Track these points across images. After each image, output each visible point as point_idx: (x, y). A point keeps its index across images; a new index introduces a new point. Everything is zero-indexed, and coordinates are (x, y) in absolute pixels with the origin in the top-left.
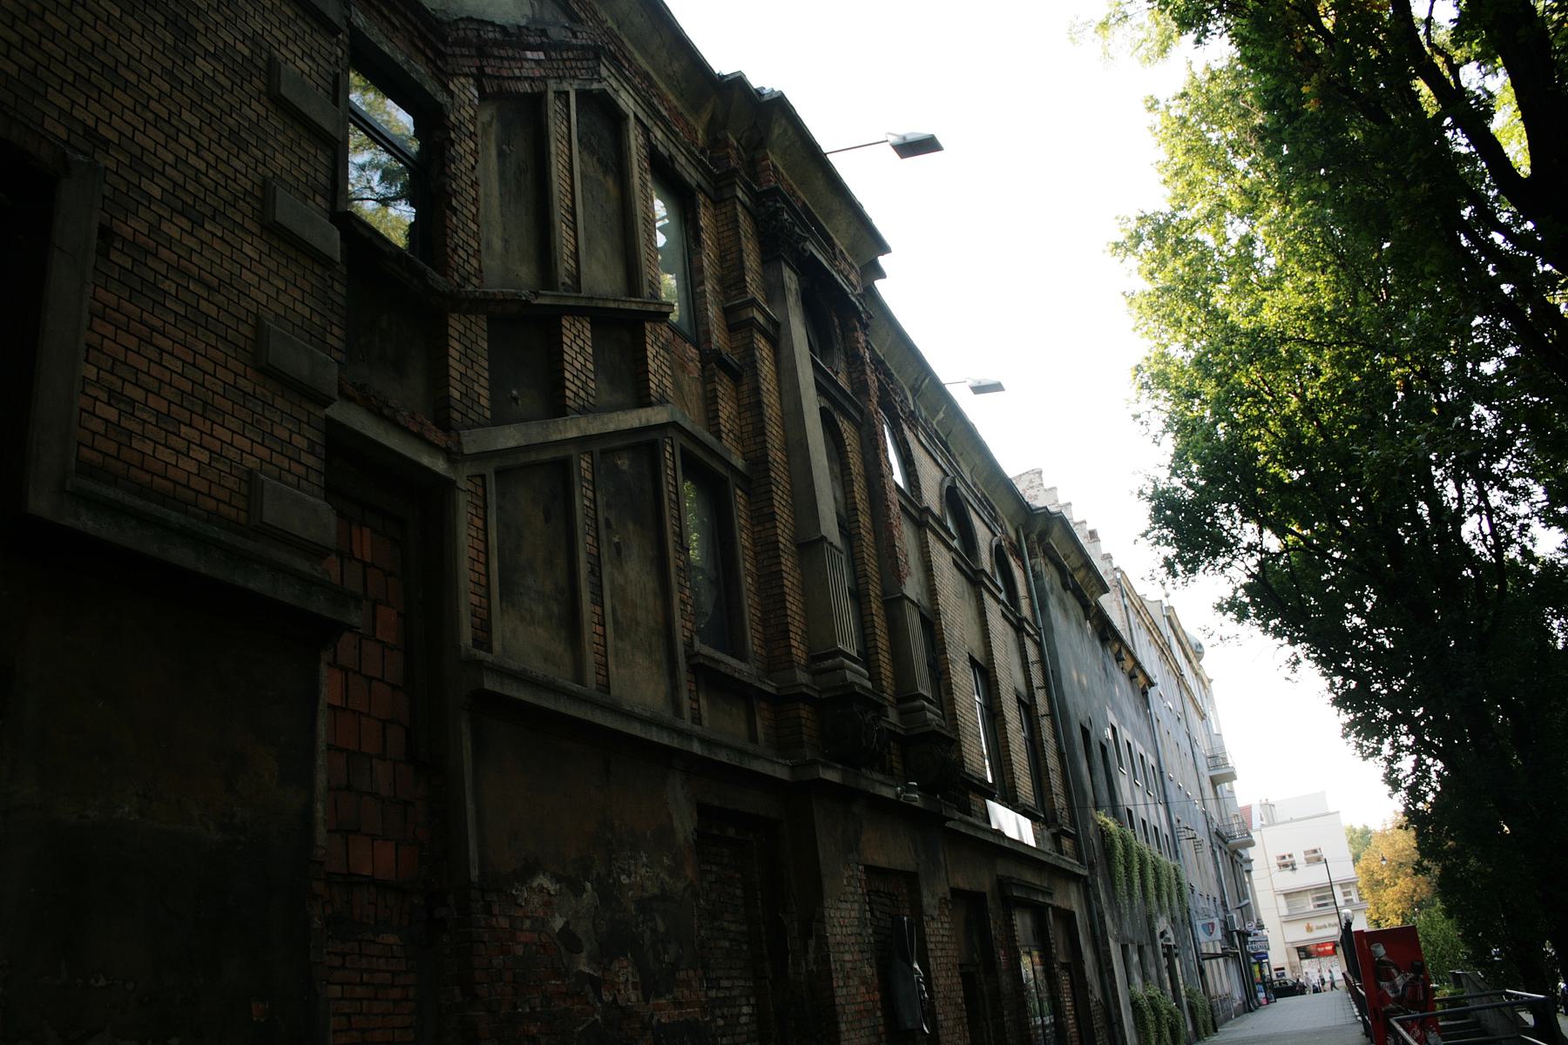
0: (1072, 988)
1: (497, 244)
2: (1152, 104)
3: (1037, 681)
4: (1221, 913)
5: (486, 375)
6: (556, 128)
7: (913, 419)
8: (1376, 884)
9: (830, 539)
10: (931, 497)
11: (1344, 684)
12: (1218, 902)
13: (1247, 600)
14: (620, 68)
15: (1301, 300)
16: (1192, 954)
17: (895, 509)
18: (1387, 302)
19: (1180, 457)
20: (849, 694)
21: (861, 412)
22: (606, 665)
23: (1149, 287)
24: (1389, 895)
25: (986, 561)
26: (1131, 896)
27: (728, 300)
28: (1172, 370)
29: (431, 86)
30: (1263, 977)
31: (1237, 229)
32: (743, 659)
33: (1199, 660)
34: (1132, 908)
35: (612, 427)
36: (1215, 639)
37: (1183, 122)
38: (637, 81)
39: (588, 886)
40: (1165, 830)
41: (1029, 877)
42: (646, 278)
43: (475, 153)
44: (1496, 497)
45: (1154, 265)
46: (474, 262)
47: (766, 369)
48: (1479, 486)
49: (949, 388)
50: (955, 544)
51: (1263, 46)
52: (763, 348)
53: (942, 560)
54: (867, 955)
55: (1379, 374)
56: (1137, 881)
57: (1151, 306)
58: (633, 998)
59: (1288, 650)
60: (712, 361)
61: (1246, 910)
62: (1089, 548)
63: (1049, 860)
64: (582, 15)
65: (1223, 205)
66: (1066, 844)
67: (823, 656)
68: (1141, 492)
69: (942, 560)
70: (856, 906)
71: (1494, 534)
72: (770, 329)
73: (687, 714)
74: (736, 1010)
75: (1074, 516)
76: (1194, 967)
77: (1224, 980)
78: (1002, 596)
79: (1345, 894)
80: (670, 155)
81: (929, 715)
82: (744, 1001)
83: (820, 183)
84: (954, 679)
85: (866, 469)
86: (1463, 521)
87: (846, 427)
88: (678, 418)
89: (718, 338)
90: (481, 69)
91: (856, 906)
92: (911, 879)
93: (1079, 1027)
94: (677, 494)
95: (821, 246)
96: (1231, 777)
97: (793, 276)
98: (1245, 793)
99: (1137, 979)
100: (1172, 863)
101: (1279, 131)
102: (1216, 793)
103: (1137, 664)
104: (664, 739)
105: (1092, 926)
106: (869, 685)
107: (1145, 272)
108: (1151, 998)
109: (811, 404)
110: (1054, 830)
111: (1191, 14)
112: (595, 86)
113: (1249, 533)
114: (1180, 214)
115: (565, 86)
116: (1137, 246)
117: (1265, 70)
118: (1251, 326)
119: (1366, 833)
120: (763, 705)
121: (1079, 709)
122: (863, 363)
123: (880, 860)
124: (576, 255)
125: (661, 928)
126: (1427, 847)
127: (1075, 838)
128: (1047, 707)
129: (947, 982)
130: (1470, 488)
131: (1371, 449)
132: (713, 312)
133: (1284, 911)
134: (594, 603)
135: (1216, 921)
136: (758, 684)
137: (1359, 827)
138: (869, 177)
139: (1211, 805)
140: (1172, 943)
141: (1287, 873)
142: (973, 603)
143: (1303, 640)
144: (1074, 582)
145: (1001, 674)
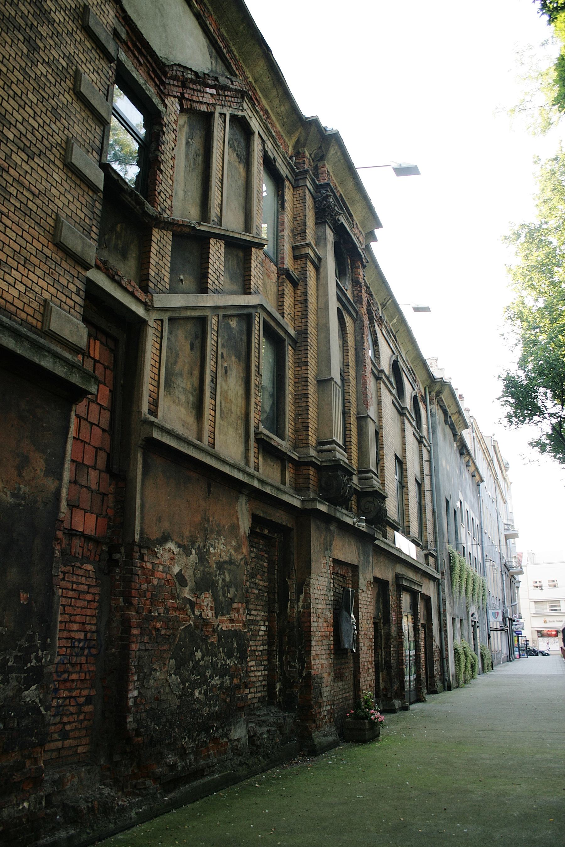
0: (425, 638)
1: (181, 194)
3: (426, 471)
4: (502, 607)
5: (169, 265)
12: (501, 601)
14: (253, 105)
16: (485, 628)
20: (337, 466)
21: (357, 313)
22: (214, 433)
25: (408, 403)
27: (295, 242)
28: (525, 312)
29: (156, 100)
32: (283, 439)
33: (506, 471)
36: (526, 461)
40: (480, 560)
41: (411, 575)
50: (394, 392)
52: (311, 269)
54: (329, 607)
56: (464, 585)
58: (210, 615)
60: (284, 274)
61: (514, 607)
62: (460, 403)
64: (237, 73)
68: (499, 377)
69: (387, 399)
70: (327, 580)
73: (252, 464)
74: (258, 628)
77: (499, 643)
78: (414, 423)
81: (375, 482)
82: (262, 623)
87: (348, 319)
91: (327, 580)
92: (355, 568)
93: (426, 660)
94: (259, 344)
95: (347, 219)
97: (332, 234)
98: (520, 546)
99: (458, 637)
102: (506, 543)
103: (477, 469)
106: (347, 461)
109: (334, 306)
115: (226, 111)
120: (290, 465)
122: (361, 287)
123: (341, 557)
125: (228, 579)
129: (367, 627)
132: (287, 248)
135: (500, 612)
136: (289, 453)
138: (377, 185)
139: (503, 548)
144: (451, 421)
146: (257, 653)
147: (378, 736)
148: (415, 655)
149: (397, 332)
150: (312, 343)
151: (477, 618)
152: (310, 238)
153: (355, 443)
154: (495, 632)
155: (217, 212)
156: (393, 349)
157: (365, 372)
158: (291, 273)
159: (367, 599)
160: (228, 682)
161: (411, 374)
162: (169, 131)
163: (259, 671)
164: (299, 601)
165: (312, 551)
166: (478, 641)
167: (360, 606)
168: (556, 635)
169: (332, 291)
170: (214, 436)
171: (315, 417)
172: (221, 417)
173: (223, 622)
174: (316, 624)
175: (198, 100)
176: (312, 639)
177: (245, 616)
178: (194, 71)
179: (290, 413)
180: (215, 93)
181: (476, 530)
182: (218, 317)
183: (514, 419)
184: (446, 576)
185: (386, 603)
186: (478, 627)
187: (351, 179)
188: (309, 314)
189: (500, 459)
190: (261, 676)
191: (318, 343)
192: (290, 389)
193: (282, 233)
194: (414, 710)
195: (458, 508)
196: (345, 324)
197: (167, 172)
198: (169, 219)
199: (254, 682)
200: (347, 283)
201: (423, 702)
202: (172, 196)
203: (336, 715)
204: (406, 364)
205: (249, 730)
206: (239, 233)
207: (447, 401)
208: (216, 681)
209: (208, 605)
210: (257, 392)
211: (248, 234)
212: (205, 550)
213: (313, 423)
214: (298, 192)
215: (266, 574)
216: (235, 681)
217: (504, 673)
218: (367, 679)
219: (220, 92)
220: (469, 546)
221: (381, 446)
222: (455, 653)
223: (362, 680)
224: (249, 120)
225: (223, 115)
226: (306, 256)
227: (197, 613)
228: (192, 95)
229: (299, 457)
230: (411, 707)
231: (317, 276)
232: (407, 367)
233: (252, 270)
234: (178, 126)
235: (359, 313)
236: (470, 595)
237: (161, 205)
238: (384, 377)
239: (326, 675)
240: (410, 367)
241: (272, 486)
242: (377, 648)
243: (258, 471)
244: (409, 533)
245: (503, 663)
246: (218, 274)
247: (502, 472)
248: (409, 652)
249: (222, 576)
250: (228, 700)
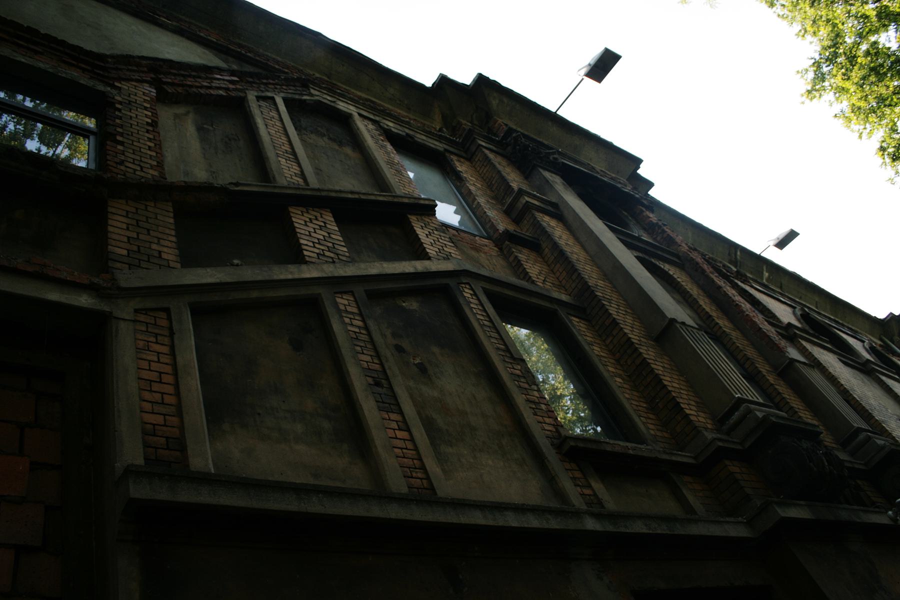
27: (503, 204)
52: (547, 221)
67: (728, 412)
80: (407, 134)
83: (554, 129)
142: (876, 386)
187: (550, 123)
193: (476, 203)
226: (528, 207)
235: (681, 254)
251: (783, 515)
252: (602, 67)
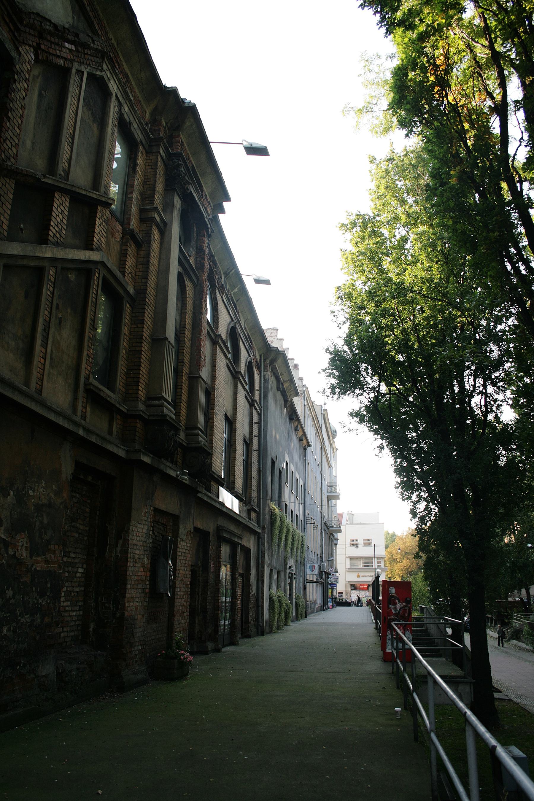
0: (243, 586)
1: (29, 144)
2: (373, 160)
3: (255, 432)
4: (319, 560)
5: (9, 212)
6: (73, 89)
7: (222, 289)
8: (393, 560)
9: (169, 340)
10: (223, 330)
11: (401, 463)
12: (319, 556)
13: (365, 413)
14: (113, 67)
15: (424, 274)
16: (302, 579)
17: (204, 332)
18: (462, 285)
19: (350, 336)
20: (163, 420)
21: (198, 279)
22: (42, 380)
23: (354, 250)
24: (398, 566)
25: (243, 368)
26: (279, 546)
27: (143, 205)
28: (355, 293)
29: (9, 46)
30: (332, 595)
31: (401, 232)
32: (113, 391)
33: (334, 438)
34: (278, 552)
35: (70, 256)
36: (346, 429)
37: (387, 172)
38: (121, 77)
39: (12, 493)
40: (301, 517)
41: (232, 528)
42: (104, 183)
43: (26, 90)
44: (490, 389)
45: (359, 240)
46: (14, 150)
47: (155, 245)
48: (485, 382)
49: (244, 277)
50: (229, 356)
51: (438, 146)
52: (156, 234)
53: (222, 362)
54: (147, 553)
55: (452, 318)
56: (283, 539)
57: (353, 259)
58: (25, 555)
59: (379, 441)
60: (129, 235)
61: (331, 563)
62: (294, 373)
63: (244, 522)
64: (100, 32)
65: (396, 218)
66: (253, 515)
67: (154, 398)
68: (328, 349)
69: (222, 362)
70: (146, 527)
71: (486, 406)
72: (162, 225)
73: (79, 413)
74: (75, 570)
75: (290, 355)
76: (302, 585)
77: (314, 594)
78: (247, 387)
79: (378, 563)
81: (201, 439)
82: (80, 565)
84: (215, 423)
85: (194, 309)
86: (473, 397)
87: (188, 284)
88: (105, 260)
89: (134, 224)
90: (39, 45)
91: (146, 527)
92: (176, 519)
93: (242, 607)
94: (96, 299)
95: (197, 189)
96: (337, 497)
97: (180, 202)
98: (342, 506)
99: (274, 587)
100: (302, 534)
101: (436, 189)
102: (328, 504)
103: (305, 434)
104: (66, 424)
105: (258, 558)
106: (174, 417)
107: (354, 242)
108: (279, 597)
109: (174, 268)
110: (249, 508)
111: (407, 120)
112: (98, 73)
113: (372, 381)
114: (378, 218)
115: (83, 68)
116: (352, 228)
117: (436, 158)
118: (398, 281)
119: (393, 535)
120: (119, 417)
121: (272, 451)
122: (204, 254)
123: (163, 507)
124: (69, 161)
125: (45, 521)
126: (423, 547)
127: (258, 513)
128: (257, 447)
129: (184, 573)
130: (480, 381)
131: (444, 350)
132: (134, 209)
133: (348, 566)
134: (42, 346)
135: (316, 565)
136: (118, 406)
137: (391, 532)
138: (229, 161)
139: (325, 508)
140: (294, 572)
141: (354, 548)
142: (232, 388)
143: (387, 438)
144: (283, 388)
145: (239, 426)
146: (73, 594)
147: (187, 674)
148: (231, 602)
149: (237, 301)
150: (149, 303)
151: (294, 570)
152: (158, 202)
153: (185, 400)
154: (311, 584)
155: (64, 166)
156: (232, 316)
157: (200, 335)
158: (136, 234)
159: (185, 547)
160: (39, 620)
161: (248, 341)
162: (21, 80)
163: (74, 611)
164: (117, 546)
165: (133, 500)
166: (294, 591)
167: (179, 554)
168: (367, 589)
169: (175, 254)
170: (42, 383)
171: (146, 373)
172: (52, 366)
173: (37, 562)
174: (132, 569)
175: (55, 53)
176: (128, 582)
177: (61, 558)
178: (53, 23)
179: (123, 368)
180: (74, 49)
181: (300, 490)
182: (56, 269)
183: (337, 390)
184: (266, 531)
185: (206, 552)
186: (295, 578)
188: (149, 275)
189: (328, 427)
190: (76, 615)
191: (155, 304)
192: (125, 344)
194: (225, 652)
195: (283, 468)
196: (185, 288)
197: (15, 121)
198: (13, 168)
199: (68, 621)
200: (191, 250)
201: (236, 645)
202: (18, 145)
203: (148, 655)
204: (243, 332)
205: (57, 667)
206: (85, 190)
207: (280, 370)
208: (26, 619)
209: (23, 545)
210: (90, 345)
211: (95, 192)
212: (24, 492)
213: (144, 379)
214: (151, 158)
215: (88, 519)
216: (47, 620)
217: (315, 621)
218: (181, 622)
219: (80, 49)
220: (292, 504)
221: (212, 406)
222: (270, 602)
223: (176, 623)
224: (107, 82)
225: (80, 73)
227: (11, 552)
228: (49, 47)
229: (128, 410)
230: (224, 650)
231: (161, 239)
232: (245, 334)
233: (96, 227)
234: (31, 75)
236: (289, 549)
237: (6, 152)
238: (220, 341)
239: (139, 617)
240: (248, 334)
241: (97, 435)
242: (193, 594)
243: (85, 420)
244: (233, 488)
245: (316, 612)
246: (60, 227)
247: (329, 438)
248: (225, 599)
249: (40, 518)
250: (38, 637)
251: (142, 459)
252: (255, 150)
